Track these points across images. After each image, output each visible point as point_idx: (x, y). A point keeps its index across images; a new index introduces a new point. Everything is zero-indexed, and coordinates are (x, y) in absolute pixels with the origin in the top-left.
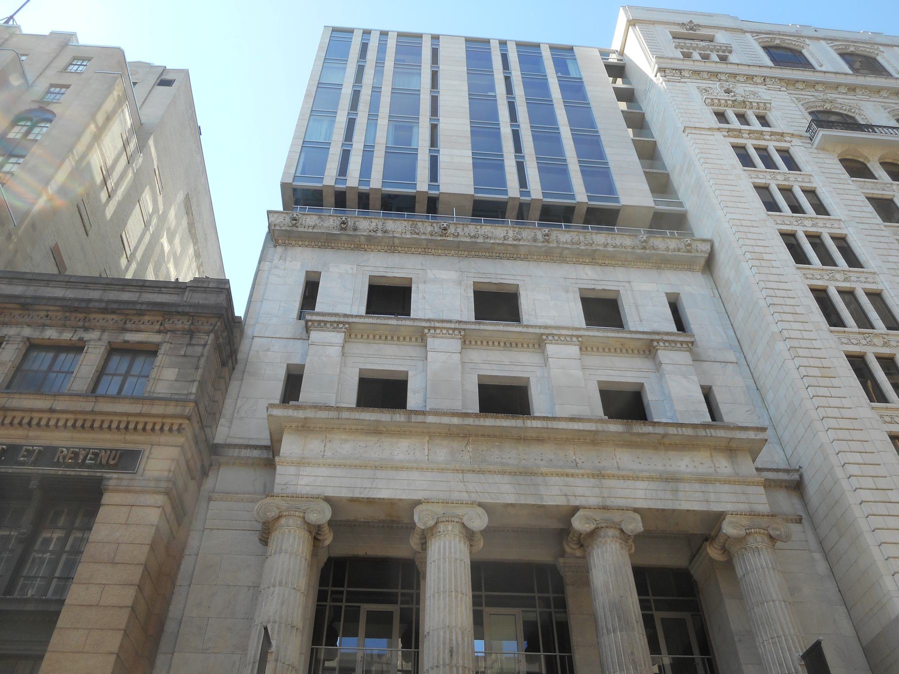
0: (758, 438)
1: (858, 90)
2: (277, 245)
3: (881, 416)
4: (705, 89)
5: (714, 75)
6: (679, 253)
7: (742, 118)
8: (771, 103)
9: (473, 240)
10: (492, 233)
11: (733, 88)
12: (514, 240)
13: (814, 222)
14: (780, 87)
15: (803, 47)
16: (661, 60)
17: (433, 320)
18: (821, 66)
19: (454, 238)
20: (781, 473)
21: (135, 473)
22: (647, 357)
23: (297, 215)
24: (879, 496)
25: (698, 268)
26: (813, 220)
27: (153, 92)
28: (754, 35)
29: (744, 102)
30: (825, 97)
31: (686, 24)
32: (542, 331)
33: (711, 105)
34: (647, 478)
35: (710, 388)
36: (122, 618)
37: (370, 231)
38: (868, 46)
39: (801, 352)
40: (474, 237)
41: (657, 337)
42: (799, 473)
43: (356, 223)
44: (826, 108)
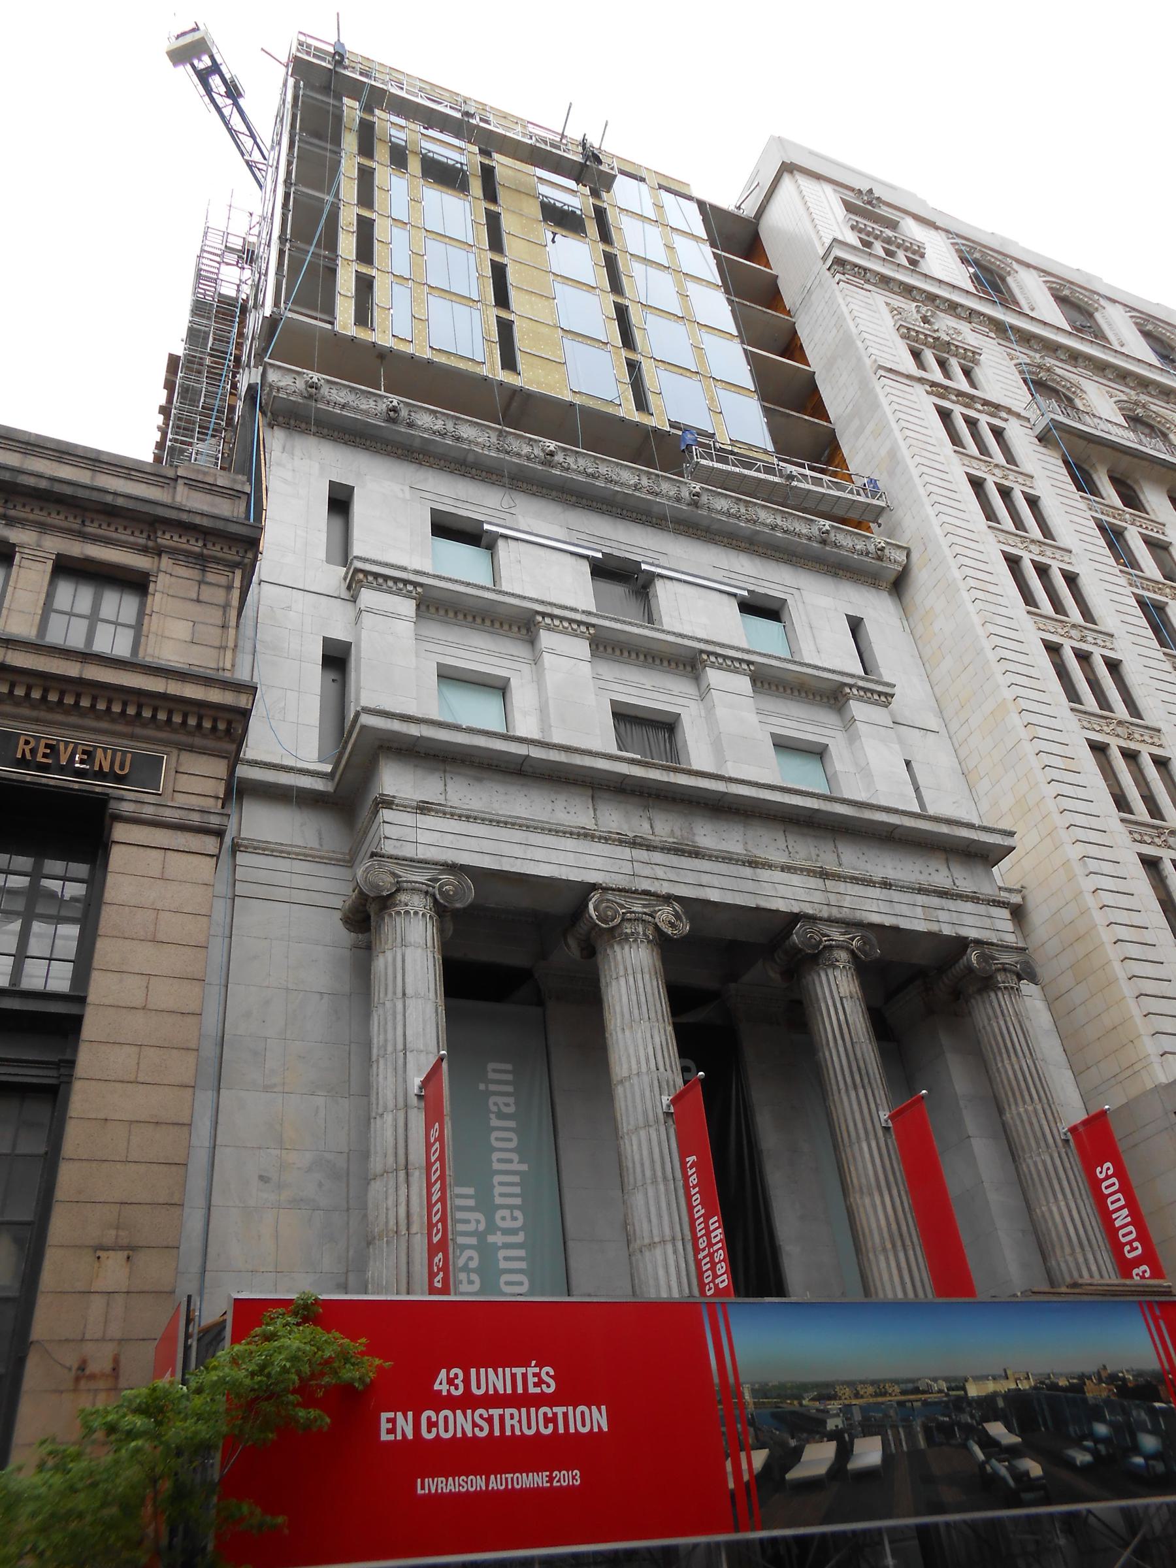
1: (1080, 360)
2: (274, 425)
3: (1130, 832)
6: (866, 559)
7: (942, 364)
9: (589, 480)
11: (932, 316)
12: (649, 493)
15: (1097, 309)
17: (551, 604)
19: (562, 471)
21: (160, 795)
22: (830, 707)
25: (885, 585)
28: (951, 236)
29: (949, 343)
31: (864, 192)
37: (434, 433)
38: (1087, 294)
39: (1042, 733)
40: (593, 476)
43: (413, 414)
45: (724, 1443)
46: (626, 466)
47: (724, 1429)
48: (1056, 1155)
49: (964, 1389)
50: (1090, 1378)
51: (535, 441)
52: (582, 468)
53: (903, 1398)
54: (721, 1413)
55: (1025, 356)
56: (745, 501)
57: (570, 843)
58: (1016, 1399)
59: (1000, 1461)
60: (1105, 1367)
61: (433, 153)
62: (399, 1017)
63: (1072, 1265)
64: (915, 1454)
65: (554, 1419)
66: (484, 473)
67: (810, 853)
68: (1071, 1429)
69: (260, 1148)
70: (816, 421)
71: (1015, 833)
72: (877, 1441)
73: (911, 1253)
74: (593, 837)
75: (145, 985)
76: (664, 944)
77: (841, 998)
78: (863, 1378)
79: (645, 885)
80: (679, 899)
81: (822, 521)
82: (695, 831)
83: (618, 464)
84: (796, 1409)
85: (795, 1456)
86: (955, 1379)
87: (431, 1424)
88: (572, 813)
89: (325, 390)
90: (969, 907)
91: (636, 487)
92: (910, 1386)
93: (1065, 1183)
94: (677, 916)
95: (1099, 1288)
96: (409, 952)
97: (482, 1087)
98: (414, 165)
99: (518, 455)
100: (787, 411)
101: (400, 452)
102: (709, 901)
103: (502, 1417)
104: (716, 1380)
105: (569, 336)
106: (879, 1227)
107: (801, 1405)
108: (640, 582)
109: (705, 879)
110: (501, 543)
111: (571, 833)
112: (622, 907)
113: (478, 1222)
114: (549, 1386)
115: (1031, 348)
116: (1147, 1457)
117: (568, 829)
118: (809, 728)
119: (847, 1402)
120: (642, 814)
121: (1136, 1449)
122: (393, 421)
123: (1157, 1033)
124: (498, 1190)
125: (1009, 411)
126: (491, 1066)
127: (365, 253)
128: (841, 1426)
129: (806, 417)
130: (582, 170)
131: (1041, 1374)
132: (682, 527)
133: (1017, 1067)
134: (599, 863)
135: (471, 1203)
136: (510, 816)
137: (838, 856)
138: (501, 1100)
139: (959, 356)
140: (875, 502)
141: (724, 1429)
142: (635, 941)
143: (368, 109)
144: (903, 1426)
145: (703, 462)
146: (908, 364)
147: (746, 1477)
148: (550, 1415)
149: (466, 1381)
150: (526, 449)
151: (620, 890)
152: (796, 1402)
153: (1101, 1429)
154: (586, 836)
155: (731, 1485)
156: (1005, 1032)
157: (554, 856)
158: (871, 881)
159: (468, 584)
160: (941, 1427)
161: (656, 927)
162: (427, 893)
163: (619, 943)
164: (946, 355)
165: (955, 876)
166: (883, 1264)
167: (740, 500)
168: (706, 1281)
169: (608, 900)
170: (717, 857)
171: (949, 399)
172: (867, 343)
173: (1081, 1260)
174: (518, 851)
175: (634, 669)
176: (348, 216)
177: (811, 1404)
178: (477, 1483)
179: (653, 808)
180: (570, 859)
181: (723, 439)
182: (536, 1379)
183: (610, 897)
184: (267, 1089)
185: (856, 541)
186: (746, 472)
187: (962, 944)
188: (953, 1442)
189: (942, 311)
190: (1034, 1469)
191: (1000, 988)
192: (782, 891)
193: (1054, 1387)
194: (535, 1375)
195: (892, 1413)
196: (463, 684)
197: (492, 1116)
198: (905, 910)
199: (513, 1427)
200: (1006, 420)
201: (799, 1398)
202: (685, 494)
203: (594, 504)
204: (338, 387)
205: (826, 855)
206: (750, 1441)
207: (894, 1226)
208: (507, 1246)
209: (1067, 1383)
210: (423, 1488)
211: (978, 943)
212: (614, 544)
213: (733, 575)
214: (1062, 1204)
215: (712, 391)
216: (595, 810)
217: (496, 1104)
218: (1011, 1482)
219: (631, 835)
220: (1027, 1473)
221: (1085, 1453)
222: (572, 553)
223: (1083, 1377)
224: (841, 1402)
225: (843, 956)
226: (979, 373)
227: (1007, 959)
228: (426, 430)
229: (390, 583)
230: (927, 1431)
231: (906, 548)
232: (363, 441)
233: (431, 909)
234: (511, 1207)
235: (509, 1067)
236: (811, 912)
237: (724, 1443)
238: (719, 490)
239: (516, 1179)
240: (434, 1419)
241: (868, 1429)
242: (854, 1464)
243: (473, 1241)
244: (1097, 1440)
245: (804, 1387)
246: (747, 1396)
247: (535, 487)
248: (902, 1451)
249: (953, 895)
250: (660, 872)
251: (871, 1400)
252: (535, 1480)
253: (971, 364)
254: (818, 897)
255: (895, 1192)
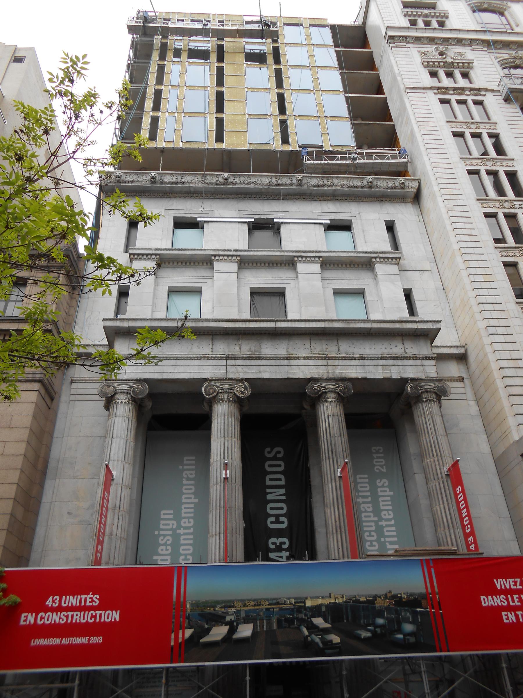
0: (434, 327)
4: (423, 53)
5: (432, 40)
8: (473, 63)
10: (261, 180)
11: (446, 50)
13: (494, 162)
14: (482, 47)
16: (410, 10)
17: (218, 250)
18: (517, 26)
20: (452, 349)
22: (368, 269)
23: (119, 173)
24: (511, 364)
25: (409, 200)
26: (494, 160)
27: (10, 66)
29: (452, 63)
30: (517, 55)
32: (294, 254)
33: (427, 67)
34: (358, 358)
35: (410, 290)
36: (19, 462)
37: (173, 183)
40: (248, 184)
41: (375, 255)
42: (465, 348)
44: (517, 64)
45: (172, 626)
46: (264, 175)
47: (174, 620)
48: (441, 482)
49: (304, 603)
50: (380, 597)
51: (219, 175)
52: (242, 182)
53: (269, 607)
54: (174, 614)
55: (507, 55)
56: (326, 177)
57: (197, 362)
58: (329, 607)
59: (317, 635)
60: (390, 592)
61: (198, 46)
62: (109, 446)
63: (444, 536)
64: (270, 632)
65: (95, 616)
66: (199, 195)
67: (322, 348)
68: (362, 621)
69: (69, 501)
70: (384, 123)
71: (440, 321)
72: (251, 626)
73: (344, 535)
74: (208, 358)
75: (4, 445)
76: (238, 401)
77: (328, 416)
78: (250, 598)
79: (232, 376)
80: (247, 380)
81: (368, 177)
82: (262, 347)
83: (260, 176)
84: (211, 612)
85: (208, 631)
86: (300, 598)
87: (42, 618)
88: (201, 348)
89: (124, 177)
90: (411, 362)
91: (270, 184)
92: (274, 601)
93: (444, 496)
94: (245, 388)
95: (409, 552)
96: (117, 419)
97: (181, 467)
98: (185, 55)
99: (212, 183)
100: (367, 122)
101: (161, 195)
102: (263, 379)
103: (72, 616)
104: (174, 599)
105: (252, 117)
106: (332, 523)
107: (214, 610)
108: (276, 227)
109: (262, 369)
110: (205, 225)
111: (197, 358)
112: (218, 387)
113: (173, 524)
114: (96, 602)
115: (511, 49)
116: (405, 635)
117: (196, 356)
118: (355, 282)
119: (238, 609)
120: (236, 343)
121: (399, 630)
122: (154, 183)
123: (516, 414)
124: (184, 510)
125: (487, 90)
126: (185, 458)
127: (156, 107)
128: (233, 619)
129: (378, 123)
130: (262, 33)
131: (350, 596)
132: (297, 197)
133: (428, 440)
134: (210, 369)
135: (171, 517)
136: (169, 355)
137: (338, 348)
138: (188, 472)
139: (465, 68)
140: (402, 160)
141: (174, 620)
142: (223, 402)
143: (165, 37)
144: (266, 620)
145: (309, 162)
146: (428, 81)
147: (180, 640)
148: (94, 614)
149: (60, 601)
150: (215, 180)
151: (217, 380)
152: (212, 609)
153: (380, 621)
154: (204, 358)
155: (172, 643)
156: (424, 423)
157: (188, 369)
158: (354, 357)
159: (179, 249)
160: (287, 620)
161: (235, 394)
162: (127, 393)
163: (217, 403)
164: (452, 69)
165: (406, 347)
166: (332, 540)
167: (324, 177)
168: (466, 523)
169: (212, 385)
170: (270, 358)
171: (449, 94)
172: (403, 76)
173: (448, 534)
174: (171, 369)
175: (264, 271)
176: (150, 92)
177: (220, 609)
178: (57, 641)
179: (242, 339)
180: (196, 369)
181: (327, 148)
182: (91, 600)
183: (213, 384)
184: (74, 478)
185: (389, 183)
186: (331, 162)
187: (404, 381)
188: (292, 626)
189: (453, 45)
190: (336, 639)
191: (424, 401)
192: (303, 369)
193: (358, 601)
194: (90, 598)
195: (262, 613)
196: (177, 293)
197: (184, 480)
198: (371, 369)
199: (76, 619)
200: (485, 95)
201: (214, 607)
202: (295, 181)
203: (253, 196)
204: (129, 174)
205: (331, 348)
206: (186, 625)
207: (338, 523)
208: (185, 534)
209: (365, 599)
210: (34, 642)
211: (412, 380)
212: (261, 213)
213: (324, 214)
214: (442, 506)
215: (324, 124)
216: (213, 345)
217: (186, 474)
218: (321, 645)
219: (227, 354)
220: (331, 641)
221: (367, 632)
222: (239, 222)
223: (375, 597)
224: (236, 609)
225: (332, 396)
226: (472, 74)
227: (429, 386)
228: (169, 183)
229: (145, 257)
230: (279, 622)
231: (418, 179)
232: (145, 194)
233: (129, 400)
234: (188, 518)
235: (194, 458)
236: (317, 377)
237: (172, 626)
238: (312, 175)
239: (192, 506)
240: (44, 616)
241: (246, 620)
242: (236, 636)
243: (170, 532)
244: (376, 626)
245: (218, 602)
246: (188, 606)
247: (223, 195)
248: (263, 630)
249: (401, 357)
250: (240, 369)
251: (252, 608)
252: (83, 640)
253: (467, 70)
254: (323, 369)
255: (340, 506)
